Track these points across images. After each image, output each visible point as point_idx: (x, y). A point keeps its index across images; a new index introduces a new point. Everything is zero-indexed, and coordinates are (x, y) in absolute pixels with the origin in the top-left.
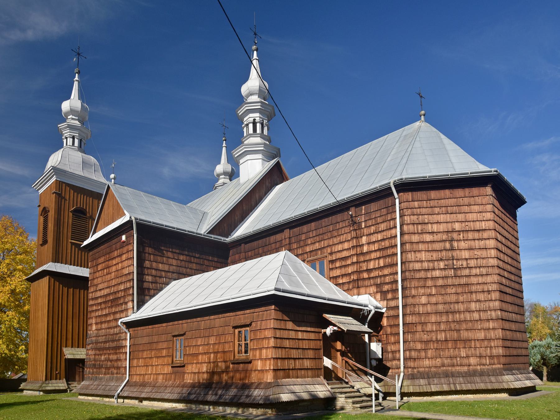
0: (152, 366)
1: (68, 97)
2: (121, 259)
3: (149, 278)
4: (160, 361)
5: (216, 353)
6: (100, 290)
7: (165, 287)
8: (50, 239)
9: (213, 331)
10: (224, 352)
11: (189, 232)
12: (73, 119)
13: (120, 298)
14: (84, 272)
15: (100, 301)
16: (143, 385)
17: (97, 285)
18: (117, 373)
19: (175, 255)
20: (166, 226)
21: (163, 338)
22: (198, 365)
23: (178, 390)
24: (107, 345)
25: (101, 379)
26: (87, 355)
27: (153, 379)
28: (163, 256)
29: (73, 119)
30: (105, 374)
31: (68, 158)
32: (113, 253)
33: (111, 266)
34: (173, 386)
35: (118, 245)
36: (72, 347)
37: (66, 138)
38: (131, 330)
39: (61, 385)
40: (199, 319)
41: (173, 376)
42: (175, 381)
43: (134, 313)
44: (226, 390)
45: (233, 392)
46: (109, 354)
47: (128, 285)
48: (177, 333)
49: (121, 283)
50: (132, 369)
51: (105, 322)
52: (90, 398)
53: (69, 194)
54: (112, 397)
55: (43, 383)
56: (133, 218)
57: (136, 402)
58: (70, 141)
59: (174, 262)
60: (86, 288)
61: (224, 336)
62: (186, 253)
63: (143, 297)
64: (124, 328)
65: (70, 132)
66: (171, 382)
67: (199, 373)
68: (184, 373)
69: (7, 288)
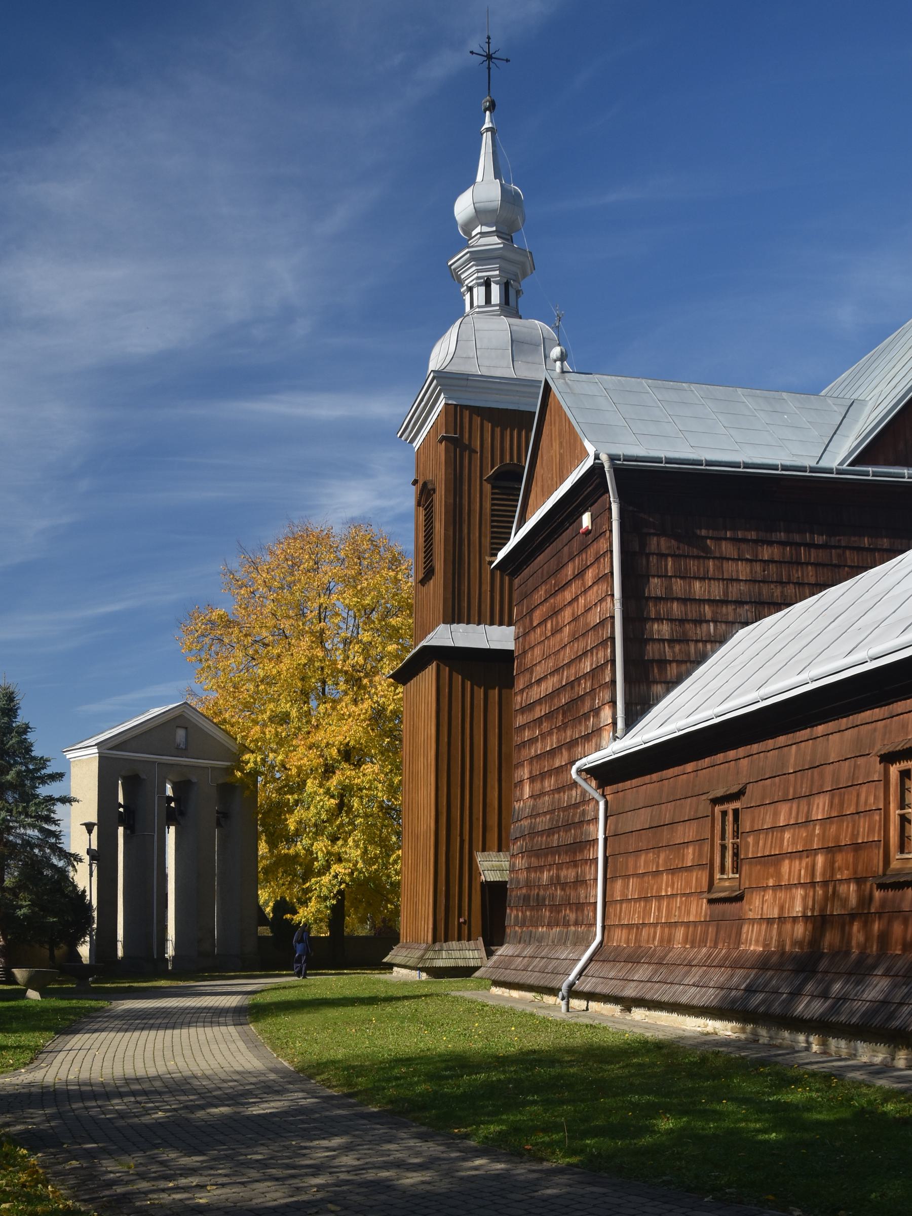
0: (659, 898)
1: (470, 180)
2: (583, 584)
3: (663, 630)
4: (680, 883)
5: (831, 851)
6: (539, 681)
7: (714, 651)
8: (439, 565)
9: (822, 776)
10: (856, 847)
11: (785, 468)
12: (483, 234)
13: (581, 698)
14: (498, 637)
15: (539, 712)
16: (634, 959)
17: (530, 670)
18: (576, 923)
19: (744, 546)
20: (710, 463)
21: (688, 808)
22: (781, 895)
23: (718, 976)
24: (555, 840)
25: (540, 939)
26: (512, 870)
27: (661, 940)
28: (706, 555)
29: (483, 234)
30: (550, 925)
31: (476, 342)
32: (564, 571)
33: (561, 609)
34: (707, 964)
35: (575, 544)
36: (499, 850)
37: (470, 289)
38: (608, 790)
39: (470, 954)
40: (782, 740)
41: (712, 930)
42: (715, 946)
43: (615, 738)
44: (858, 983)
45: (876, 988)
46: (560, 866)
47: (601, 656)
48: (720, 792)
49: (585, 654)
50: (611, 910)
51: (550, 773)
52: (515, 994)
53: (482, 436)
54: (553, 991)
55: (427, 950)
56: (604, 458)
57: (613, 1010)
58: (479, 293)
59: (743, 570)
60: (508, 682)
61: (853, 790)
62: (782, 536)
63: (644, 687)
64: (590, 788)
65: (478, 271)
66: (704, 950)
67: (781, 920)
68: (741, 920)
69: (366, 705)
